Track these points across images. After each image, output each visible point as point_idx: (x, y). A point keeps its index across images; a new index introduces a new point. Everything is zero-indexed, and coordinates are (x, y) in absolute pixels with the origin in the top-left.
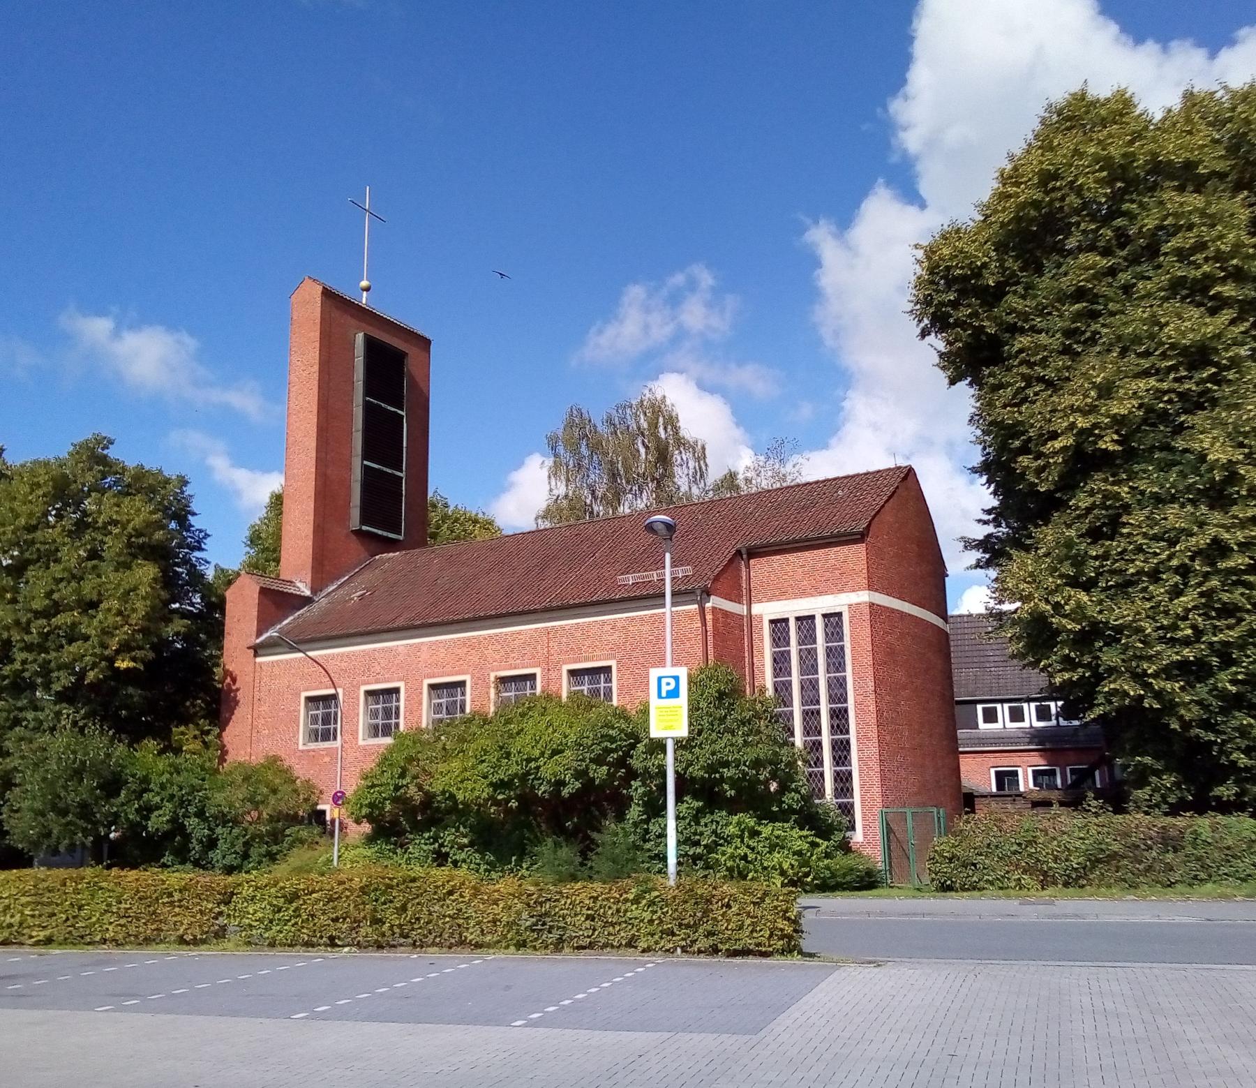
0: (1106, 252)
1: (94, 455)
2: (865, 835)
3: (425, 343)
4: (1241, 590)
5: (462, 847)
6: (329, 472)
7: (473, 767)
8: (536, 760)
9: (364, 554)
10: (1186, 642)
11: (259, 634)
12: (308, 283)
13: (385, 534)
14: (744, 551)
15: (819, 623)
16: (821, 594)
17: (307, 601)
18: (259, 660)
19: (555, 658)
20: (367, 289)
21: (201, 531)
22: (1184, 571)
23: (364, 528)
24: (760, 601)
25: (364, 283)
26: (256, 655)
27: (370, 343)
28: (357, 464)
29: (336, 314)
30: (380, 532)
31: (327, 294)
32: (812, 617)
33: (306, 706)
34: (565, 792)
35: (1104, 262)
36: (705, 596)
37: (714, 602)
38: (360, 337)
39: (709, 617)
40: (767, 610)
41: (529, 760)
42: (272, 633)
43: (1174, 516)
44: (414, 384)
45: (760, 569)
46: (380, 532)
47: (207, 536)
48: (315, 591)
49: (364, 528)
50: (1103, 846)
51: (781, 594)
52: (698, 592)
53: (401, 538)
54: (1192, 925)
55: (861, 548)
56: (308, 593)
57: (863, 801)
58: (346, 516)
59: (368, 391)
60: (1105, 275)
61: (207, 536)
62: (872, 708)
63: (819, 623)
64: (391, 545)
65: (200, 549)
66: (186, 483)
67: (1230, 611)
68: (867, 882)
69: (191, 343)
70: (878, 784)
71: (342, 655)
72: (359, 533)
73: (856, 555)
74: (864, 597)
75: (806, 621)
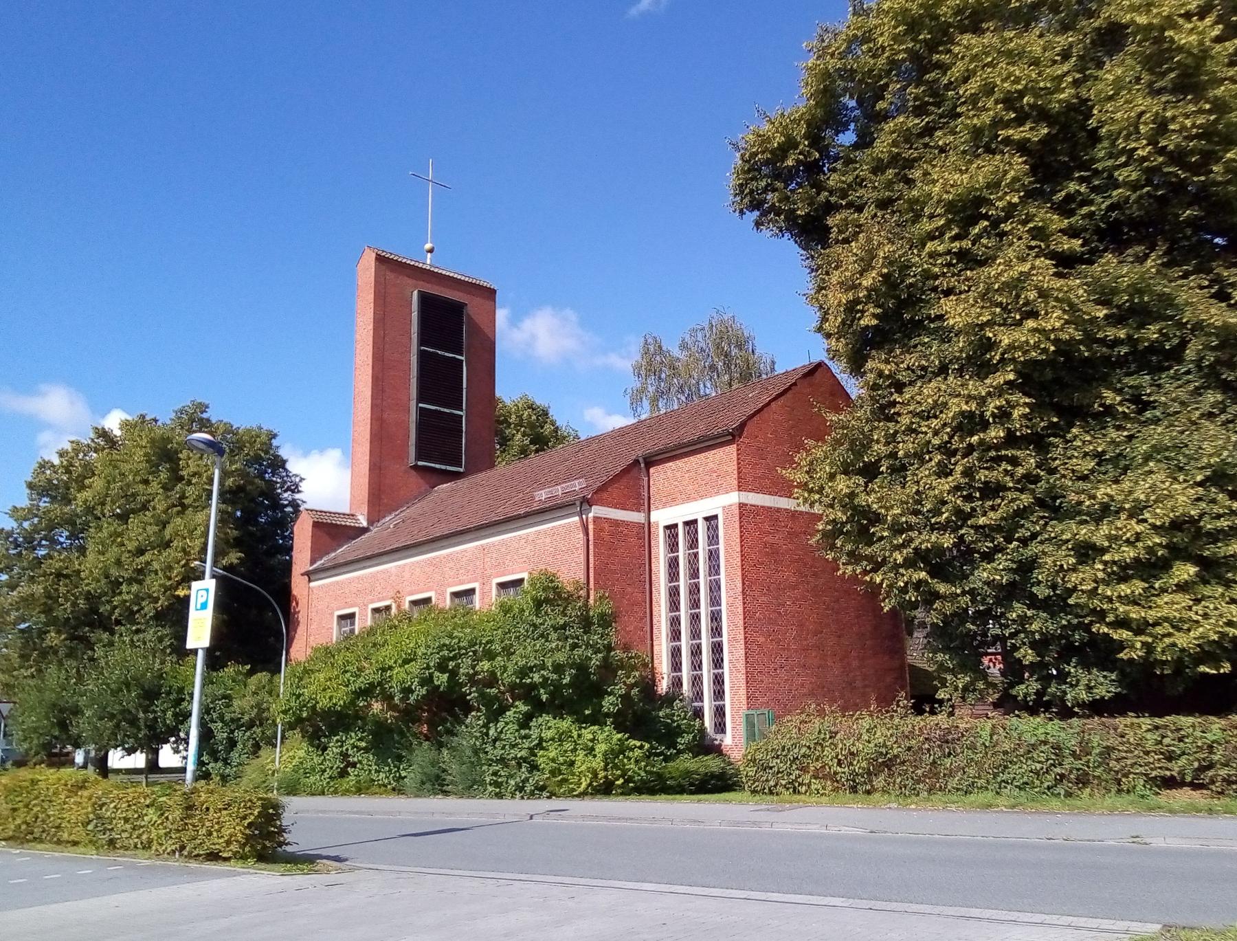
0: (919, 111)
1: (195, 418)
2: (734, 737)
3: (489, 294)
4: (1004, 465)
5: (359, 749)
6: (385, 416)
7: (337, 677)
8: (391, 668)
9: (425, 486)
10: (943, 528)
11: (312, 563)
12: (367, 250)
13: (443, 467)
14: (641, 460)
15: (702, 527)
16: (702, 497)
17: (364, 530)
18: (312, 584)
19: (488, 572)
20: (431, 251)
21: (296, 476)
22: (946, 449)
23: (420, 463)
24: (657, 508)
25: (428, 246)
26: (310, 581)
27: (425, 299)
28: (413, 403)
29: (391, 276)
30: (438, 466)
31: (380, 259)
32: (695, 521)
33: (338, 623)
34: (413, 698)
35: (915, 123)
36: (585, 506)
37: (597, 511)
38: (416, 293)
39: (591, 527)
40: (661, 517)
41: (384, 670)
42: (318, 563)
43: (929, 391)
44: (476, 330)
45: (661, 477)
46: (438, 466)
47: (302, 479)
48: (371, 522)
49: (420, 463)
50: (884, 750)
51: (671, 501)
52: (578, 503)
53: (461, 470)
54: (855, 839)
55: (732, 449)
56: (365, 524)
57: (732, 704)
58: (403, 455)
59: (422, 341)
60: (921, 135)
61: (302, 479)
62: (740, 610)
63: (702, 527)
64: (456, 476)
65: (299, 492)
66: (275, 436)
67: (992, 491)
68: (720, 783)
69: (570, 314)
70: (744, 686)
71: (358, 578)
72: (415, 467)
73: (725, 458)
74: (734, 498)
75: (691, 524)
